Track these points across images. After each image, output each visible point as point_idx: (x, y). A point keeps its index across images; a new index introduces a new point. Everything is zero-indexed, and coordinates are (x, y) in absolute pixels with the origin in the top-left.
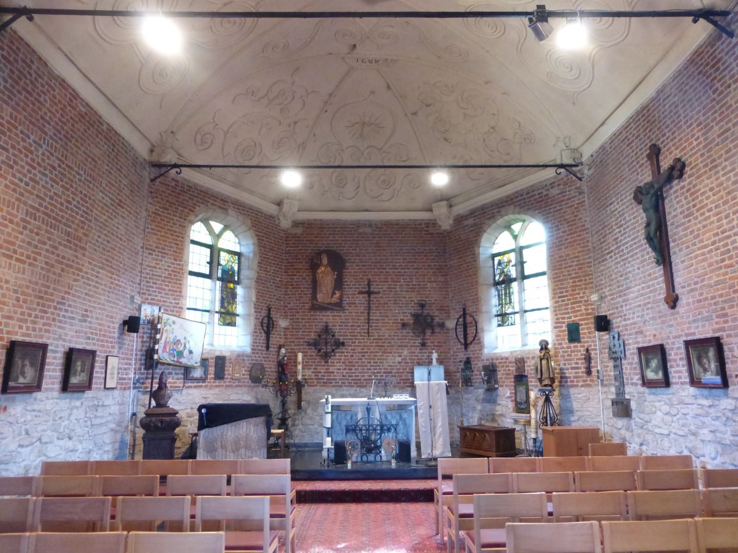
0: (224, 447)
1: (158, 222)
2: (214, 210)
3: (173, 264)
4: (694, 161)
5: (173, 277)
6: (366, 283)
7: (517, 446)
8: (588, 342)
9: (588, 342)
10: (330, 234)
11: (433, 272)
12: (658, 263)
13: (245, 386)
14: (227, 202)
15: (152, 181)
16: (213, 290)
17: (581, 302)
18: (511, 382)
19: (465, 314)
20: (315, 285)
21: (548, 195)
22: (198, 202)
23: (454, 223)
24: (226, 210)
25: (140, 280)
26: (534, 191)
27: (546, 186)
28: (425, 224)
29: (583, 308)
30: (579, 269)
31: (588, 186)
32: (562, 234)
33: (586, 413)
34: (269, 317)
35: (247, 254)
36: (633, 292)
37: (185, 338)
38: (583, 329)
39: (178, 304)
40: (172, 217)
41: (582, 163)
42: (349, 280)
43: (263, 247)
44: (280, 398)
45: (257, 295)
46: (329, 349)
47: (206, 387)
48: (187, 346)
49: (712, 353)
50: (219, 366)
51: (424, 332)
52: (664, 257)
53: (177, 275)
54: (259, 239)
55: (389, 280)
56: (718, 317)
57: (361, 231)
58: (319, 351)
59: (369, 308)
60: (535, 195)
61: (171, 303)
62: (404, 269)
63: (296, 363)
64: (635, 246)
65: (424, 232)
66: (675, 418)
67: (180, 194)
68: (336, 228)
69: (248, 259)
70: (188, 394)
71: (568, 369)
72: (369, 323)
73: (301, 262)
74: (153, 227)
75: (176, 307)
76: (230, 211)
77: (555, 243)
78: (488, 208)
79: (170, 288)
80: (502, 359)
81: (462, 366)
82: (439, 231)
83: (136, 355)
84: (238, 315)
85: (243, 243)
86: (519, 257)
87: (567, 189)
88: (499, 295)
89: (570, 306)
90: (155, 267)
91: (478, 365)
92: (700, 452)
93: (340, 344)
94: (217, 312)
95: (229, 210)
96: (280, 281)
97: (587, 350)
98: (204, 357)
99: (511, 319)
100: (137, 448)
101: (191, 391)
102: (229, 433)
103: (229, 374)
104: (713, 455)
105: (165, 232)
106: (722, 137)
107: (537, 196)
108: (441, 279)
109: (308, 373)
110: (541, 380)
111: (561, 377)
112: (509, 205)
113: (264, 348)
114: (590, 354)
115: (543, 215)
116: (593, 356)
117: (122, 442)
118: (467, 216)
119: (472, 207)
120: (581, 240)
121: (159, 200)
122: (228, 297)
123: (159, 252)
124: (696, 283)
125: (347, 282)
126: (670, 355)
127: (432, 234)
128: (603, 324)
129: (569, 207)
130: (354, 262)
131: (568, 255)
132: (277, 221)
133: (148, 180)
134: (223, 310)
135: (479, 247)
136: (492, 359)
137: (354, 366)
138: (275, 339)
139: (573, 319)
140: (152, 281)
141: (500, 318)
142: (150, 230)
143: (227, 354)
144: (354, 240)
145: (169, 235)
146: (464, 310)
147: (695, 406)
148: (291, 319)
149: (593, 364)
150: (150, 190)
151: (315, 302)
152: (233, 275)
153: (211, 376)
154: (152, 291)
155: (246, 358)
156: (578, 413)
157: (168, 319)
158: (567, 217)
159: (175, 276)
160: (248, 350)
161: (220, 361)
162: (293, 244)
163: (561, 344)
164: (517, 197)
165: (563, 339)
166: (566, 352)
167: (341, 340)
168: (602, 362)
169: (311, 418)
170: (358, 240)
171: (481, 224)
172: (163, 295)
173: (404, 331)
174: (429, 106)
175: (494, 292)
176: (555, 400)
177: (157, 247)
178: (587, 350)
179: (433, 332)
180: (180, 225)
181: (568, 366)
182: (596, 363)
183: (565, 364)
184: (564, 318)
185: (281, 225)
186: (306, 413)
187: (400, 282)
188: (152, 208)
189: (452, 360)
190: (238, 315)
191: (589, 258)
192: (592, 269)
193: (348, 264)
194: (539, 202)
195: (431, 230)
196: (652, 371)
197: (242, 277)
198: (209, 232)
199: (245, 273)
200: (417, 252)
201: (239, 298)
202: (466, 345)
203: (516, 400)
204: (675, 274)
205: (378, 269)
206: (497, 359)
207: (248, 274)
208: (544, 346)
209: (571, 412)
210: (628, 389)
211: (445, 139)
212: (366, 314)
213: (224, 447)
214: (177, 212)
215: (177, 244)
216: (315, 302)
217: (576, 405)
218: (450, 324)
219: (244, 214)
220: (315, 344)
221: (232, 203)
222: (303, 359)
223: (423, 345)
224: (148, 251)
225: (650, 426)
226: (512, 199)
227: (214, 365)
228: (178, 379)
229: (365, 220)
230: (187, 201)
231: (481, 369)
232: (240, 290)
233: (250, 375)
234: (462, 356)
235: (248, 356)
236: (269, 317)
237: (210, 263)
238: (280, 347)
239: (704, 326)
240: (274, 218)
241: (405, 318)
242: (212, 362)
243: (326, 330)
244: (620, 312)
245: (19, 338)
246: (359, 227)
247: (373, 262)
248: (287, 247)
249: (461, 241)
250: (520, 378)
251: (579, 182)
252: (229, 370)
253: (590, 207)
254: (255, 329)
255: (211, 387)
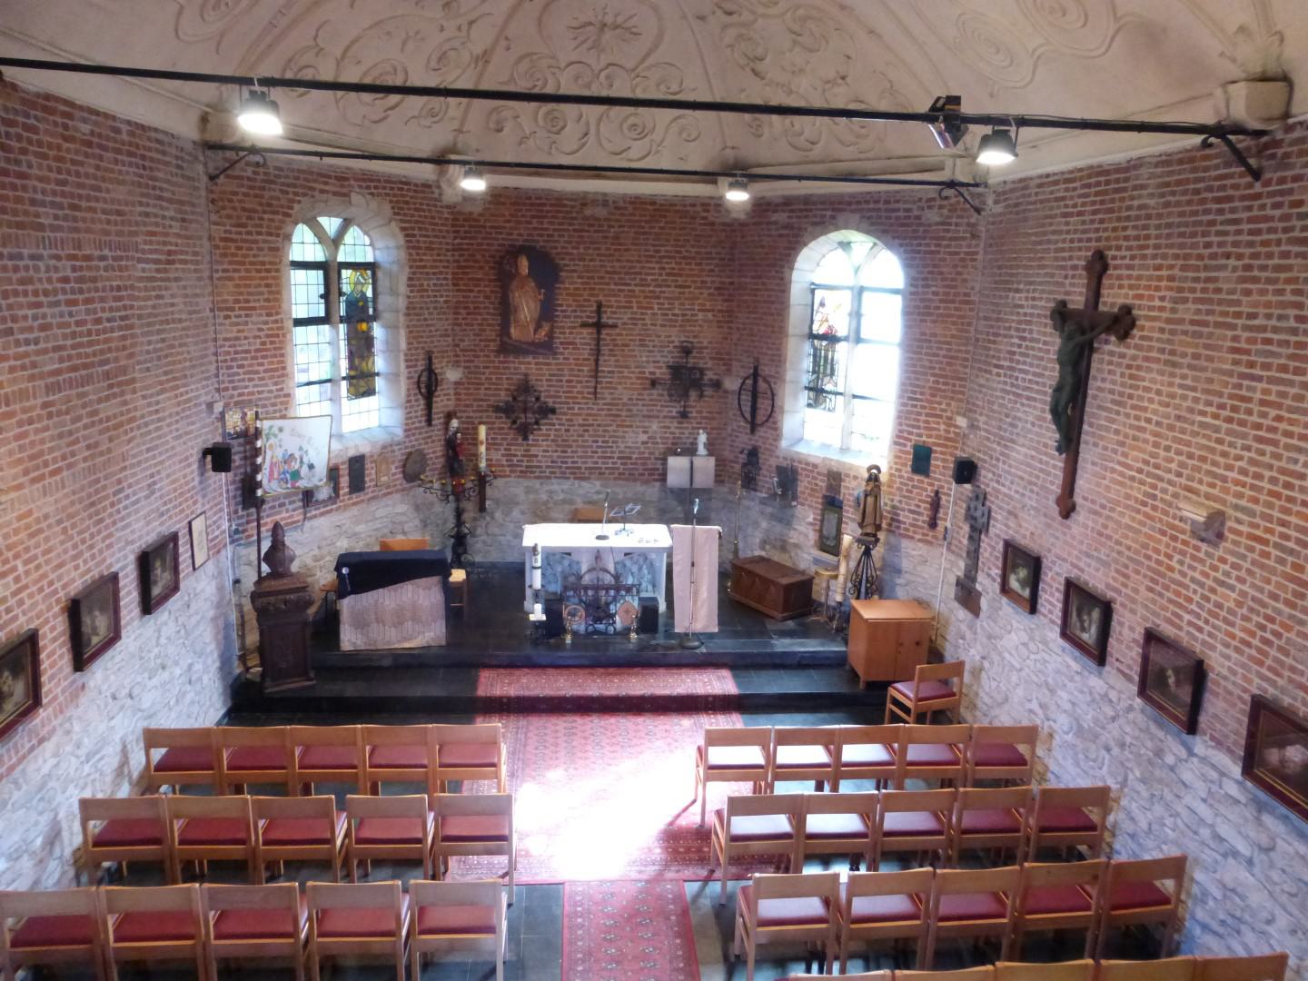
0: (380, 621)
1: (233, 255)
2: (326, 202)
3: (266, 323)
4: (1148, 328)
5: (268, 346)
6: (594, 308)
7: (814, 596)
8: (939, 480)
9: (939, 480)
10: (533, 217)
11: (710, 294)
12: (1059, 449)
13: (397, 491)
14: (346, 179)
15: (212, 178)
16: (333, 343)
17: (941, 417)
18: (817, 502)
19: (755, 375)
20: (506, 311)
21: (918, 217)
22: (296, 194)
23: (754, 211)
24: (346, 195)
25: (217, 368)
26: (898, 201)
27: (920, 200)
28: (703, 205)
29: (942, 427)
30: (948, 364)
31: (987, 231)
32: (930, 296)
33: (919, 580)
34: (430, 370)
35: (388, 266)
36: (1018, 452)
37: (301, 449)
38: (937, 459)
39: (282, 389)
40: (255, 237)
41: (986, 185)
42: (564, 302)
43: (414, 248)
44: (452, 505)
45: (408, 338)
46: (531, 418)
47: (337, 509)
48: (305, 460)
49: (1096, 614)
50: (353, 474)
51: (686, 395)
52: (1070, 443)
53: (273, 351)
54: (407, 236)
55: (635, 305)
56: (1117, 571)
57: (588, 212)
58: (514, 422)
59: (598, 352)
60: (898, 210)
61: (270, 391)
62: (660, 286)
63: (475, 442)
64: (1036, 387)
65: (699, 221)
66: (1032, 657)
67: (263, 189)
68: (544, 205)
69: (390, 274)
70: (312, 528)
71: (903, 510)
72: (596, 377)
73: (481, 268)
74: (225, 266)
75: (279, 396)
76: (355, 198)
77: (918, 307)
78: (815, 203)
79: (266, 367)
80: (807, 464)
81: (743, 458)
82: (727, 220)
83: (228, 491)
84: (378, 374)
85: (379, 244)
86: (856, 304)
87: (954, 220)
88: (815, 356)
89: (923, 418)
90: (237, 339)
91: (769, 464)
92: (1053, 716)
93: (547, 411)
94: (344, 378)
95: (353, 195)
96: (446, 302)
97: (937, 493)
98: (333, 462)
99: (831, 401)
100: (248, 627)
101: (315, 523)
102: (387, 602)
103: (371, 480)
104: (1065, 729)
105: (248, 271)
106: (1196, 328)
107: (901, 214)
108: (720, 305)
109: (496, 456)
110: (861, 525)
111: (892, 519)
112: (853, 211)
113: (423, 424)
114: (939, 499)
115: (905, 252)
116: (943, 502)
117: (227, 626)
118: (777, 205)
119: (787, 193)
120: (959, 317)
121: (229, 211)
122: (360, 347)
123: (240, 309)
124: (1103, 507)
125: (561, 305)
126: (1046, 575)
127: (713, 224)
128: (966, 471)
129: (951, 254)
130: (575, 271)
131: (935, 335)
132: (437, 191)
133: (205, 179)
134: (353, 373)
135: (792, 269)
136: (793, 460)
137: (570, 446)
138: (442, 403)
139: (924, 439)
140: (234, 364)
141: (812, 394)
142: (220, 274)
143: (365, 449)
144: (575, 230)
145: (254, 274)
146: (756, 369)
147: (1059, 659)
148: (466, 367)
149: (941, 515)
150: (212, 196)
151: (505, 339)
152: (365, 308)
153: (344, 490)
154: (239, 381)
155: (396, 448)
156: (907, 576)
157: (271, 427)
158: (945, 270)
159: (272, 343)
160: (399, 432)
161: (357, 463)
162: (466, 232)
163: (899, 470)
164: (867, 202)
165: (905, 465)
166: (906, 485)
167: (550, 405)
168: (953, 516)
169: (501, 525)
170: (581, 231)
171: (800, 229)
172: (256, 382)
173: (655, 392)
174: (730, 14)
175: (807, 348)
176: (877, 552)
177: (237, 301)
178: (937, 493)
179: (701, 396)
180: (271, 249)
181: (903, 505)
182: (946, 514)
183: (900, 502)
184: (911, 433)
185: (444, 198)
186: (493, 518)
187: (652, 308)
188: (218, 231)
189: (728, 442)
190: (378, 374)
191: (967, 352)
192: (968, 371)
193: (563, 274)
194: (903, 225)
195: (711, 216)
196: (1018, 580)
197: (380, 307)
198: (319, 238)
199: (385, 301)
200: (684, 258)
201: (378, 345)
202: (754, 427)
203: (821, 531)
204: (1079, 472)
205: (616, 284)
206: (800, 462)
207: (394, 301)
208: (874, 479)
209: (899, 571)
210: (981, 577)
211: (753, 70)
212: (593, 363)
213: (380, 621)
214: (261, 226)
215: (268, 274)
216: (505, 339)
217: (905, 564)
218: (732, 384)
219: (379, 195)
220: (506, 410)
221: (356, 180)
222: (487, 434)
223: (684, 415)
224: (222, 314)
225: (999, 644)
226: (859, 203)
227: (346, 472)
228: (294, 510)
229: (596, 193)
230: (278, 199)
231: (774, 469)
232: (378, 331)
233: (404, 472)
234: (744, 440)
235: (399, 444)
236: (430, 370)
237: (326, 296)
238: (449, 416)
239: (1098, 570)
240: (430, 186)
241: (658, 371)
242: (344, 470)
243: (525, 387)
244: (994, 466)
245: (76, 587)
246: (584, 205)
247: (607, 272)
248: (455, 238)
249: (763, 247)
250: (832, 503)
251: (976, 215)
252: (370, 472)
253: (984, 267)
254: (408, 395)
255: (346, 507)
